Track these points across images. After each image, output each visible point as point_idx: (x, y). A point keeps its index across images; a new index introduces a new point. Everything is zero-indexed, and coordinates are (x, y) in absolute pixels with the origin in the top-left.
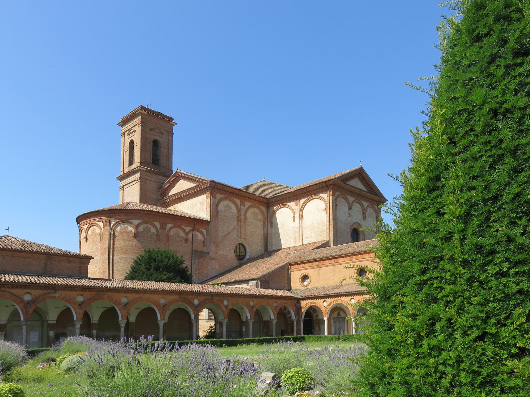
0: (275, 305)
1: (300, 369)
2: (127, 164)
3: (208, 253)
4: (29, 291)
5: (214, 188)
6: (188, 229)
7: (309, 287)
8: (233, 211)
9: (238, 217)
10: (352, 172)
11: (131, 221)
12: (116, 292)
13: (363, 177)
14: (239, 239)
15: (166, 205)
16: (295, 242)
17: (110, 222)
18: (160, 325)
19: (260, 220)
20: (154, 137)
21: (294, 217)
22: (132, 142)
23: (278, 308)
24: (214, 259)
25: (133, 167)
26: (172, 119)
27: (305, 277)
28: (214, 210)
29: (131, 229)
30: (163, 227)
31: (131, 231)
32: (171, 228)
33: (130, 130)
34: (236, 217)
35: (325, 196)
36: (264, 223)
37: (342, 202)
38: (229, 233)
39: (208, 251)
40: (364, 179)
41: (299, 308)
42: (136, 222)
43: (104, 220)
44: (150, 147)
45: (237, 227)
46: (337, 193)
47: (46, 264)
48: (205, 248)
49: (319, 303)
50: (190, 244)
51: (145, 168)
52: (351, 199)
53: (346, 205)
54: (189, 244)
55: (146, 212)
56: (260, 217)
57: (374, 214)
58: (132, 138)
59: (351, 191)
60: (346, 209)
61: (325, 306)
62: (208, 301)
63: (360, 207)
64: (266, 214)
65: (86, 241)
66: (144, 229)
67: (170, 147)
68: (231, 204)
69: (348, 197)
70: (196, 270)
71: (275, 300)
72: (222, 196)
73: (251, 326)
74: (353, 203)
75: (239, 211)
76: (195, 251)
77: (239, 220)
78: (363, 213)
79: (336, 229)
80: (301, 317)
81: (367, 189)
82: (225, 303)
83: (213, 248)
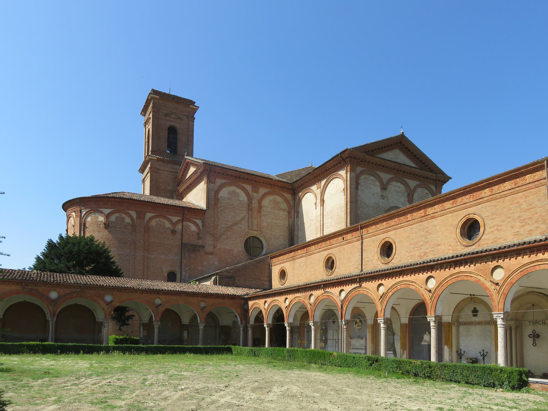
1: (56, 398)
3: (203, 247)
6: (175, 219)
8: (241, 199)
9: (249, 205)
11: (101, 210)
14: (251, 232)
16: (316, 233)
17: (81, 211)
18: (155, 326)
19: (284, 210)
20: (169, 124)
26: (193, 103)
27: (283, 274)
28: (212, 197)
29: (101, 219)
30: (141, 216)
31: (102, 221)
32: (151, 219)
35: (342, 173)
36: (289, 212)
38: (236, 224)
40: (409, 150)
42: (107, 211)
43: (75, 210)
44: (164, 134)
45: (247, 217)
46: (359, 169)
48: (200, 241)
51: (155, 157)
52: (385, 177)
53: (378, 184)
54: (178, 236)
55: (117, 200)
56: (284, 206)
60: (376, 188)
63: (404, 188)
64: (291, 202)
71: (201, 299)
72: (224, 181)
73: (156, 330)
74: (389, 181)
75: (250, 198)
76: (186, 244)
78: (408, 195)
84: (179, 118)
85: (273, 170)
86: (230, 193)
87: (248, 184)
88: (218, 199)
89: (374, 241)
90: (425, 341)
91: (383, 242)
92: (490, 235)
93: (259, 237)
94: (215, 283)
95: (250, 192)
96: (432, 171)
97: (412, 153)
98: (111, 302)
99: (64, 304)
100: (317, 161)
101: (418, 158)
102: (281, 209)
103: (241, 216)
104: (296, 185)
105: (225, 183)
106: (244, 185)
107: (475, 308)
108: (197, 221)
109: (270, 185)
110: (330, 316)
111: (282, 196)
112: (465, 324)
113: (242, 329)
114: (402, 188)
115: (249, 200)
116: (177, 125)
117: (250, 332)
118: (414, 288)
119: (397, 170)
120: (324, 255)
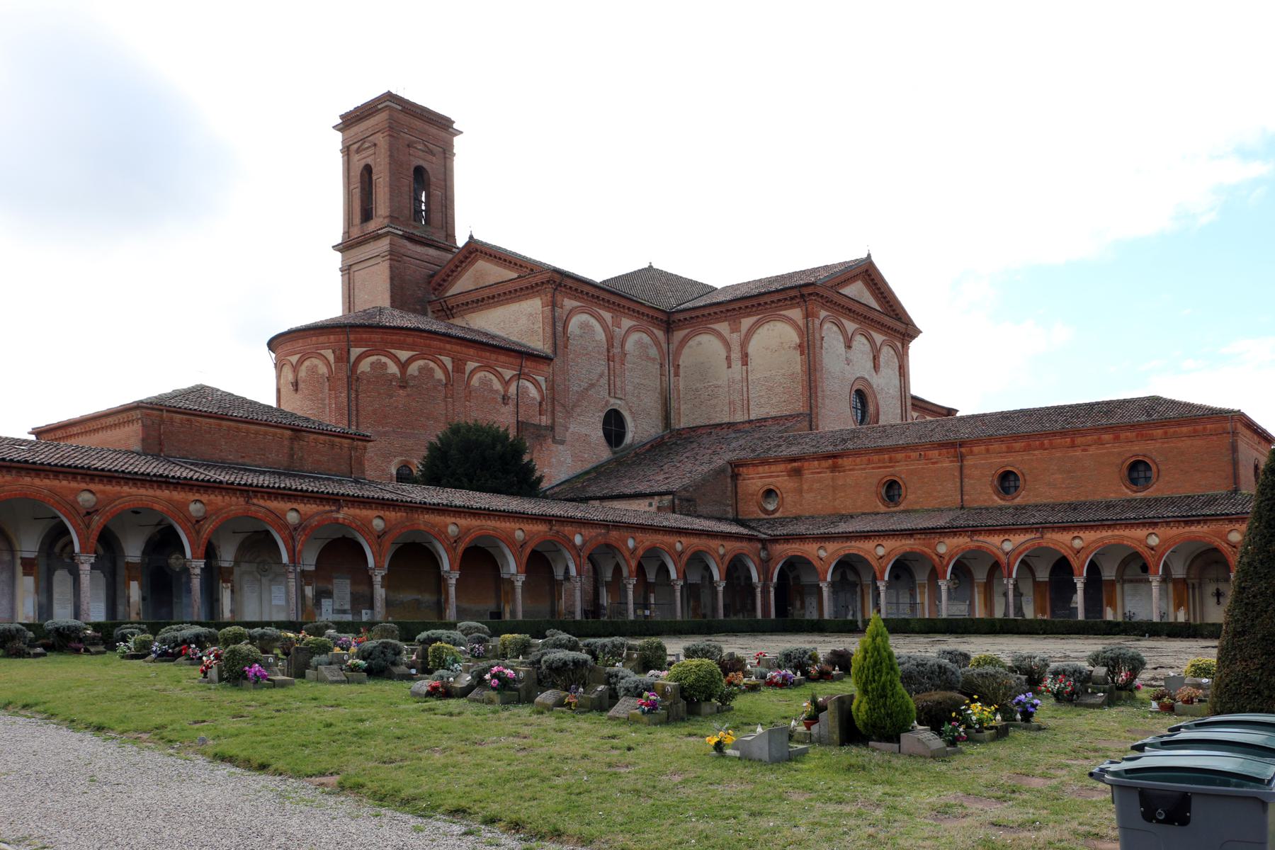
0: (722, 551)
2: (357, 219)
4: (296, 506)
5: (560, 285)
6: (508, 373)
7: (777, 515)
9: (608, 351)
10: (886, 284)
14: (612, 401)
15: (447, 312)
21: (728, 358)
22: (368, 170)
23: (727, 559)
25: (372, 226)
30: (459, 368)
32: (473, 372)
38: (592, 386)
47: (292, 449)
48: (544, 418)
49: (811, 550)
52: (850, 326)
54: (510, 408)
56: (653, 352)
58: (369, 161)
61: (825, 555)
64: (665, 346)
65: (296, 390)
66: (421, 369)
68: (593, 321)
69: (873, 334)
71: (720, 542)
77: (610, 359)
78: (874, 358)
87: (608, 309)
99: (120, 544)
103: (599, 370)
108: (539, 378)
111: (651, 335)
112: (1131, 581)
114: (867, 347)
120: (884, 473)
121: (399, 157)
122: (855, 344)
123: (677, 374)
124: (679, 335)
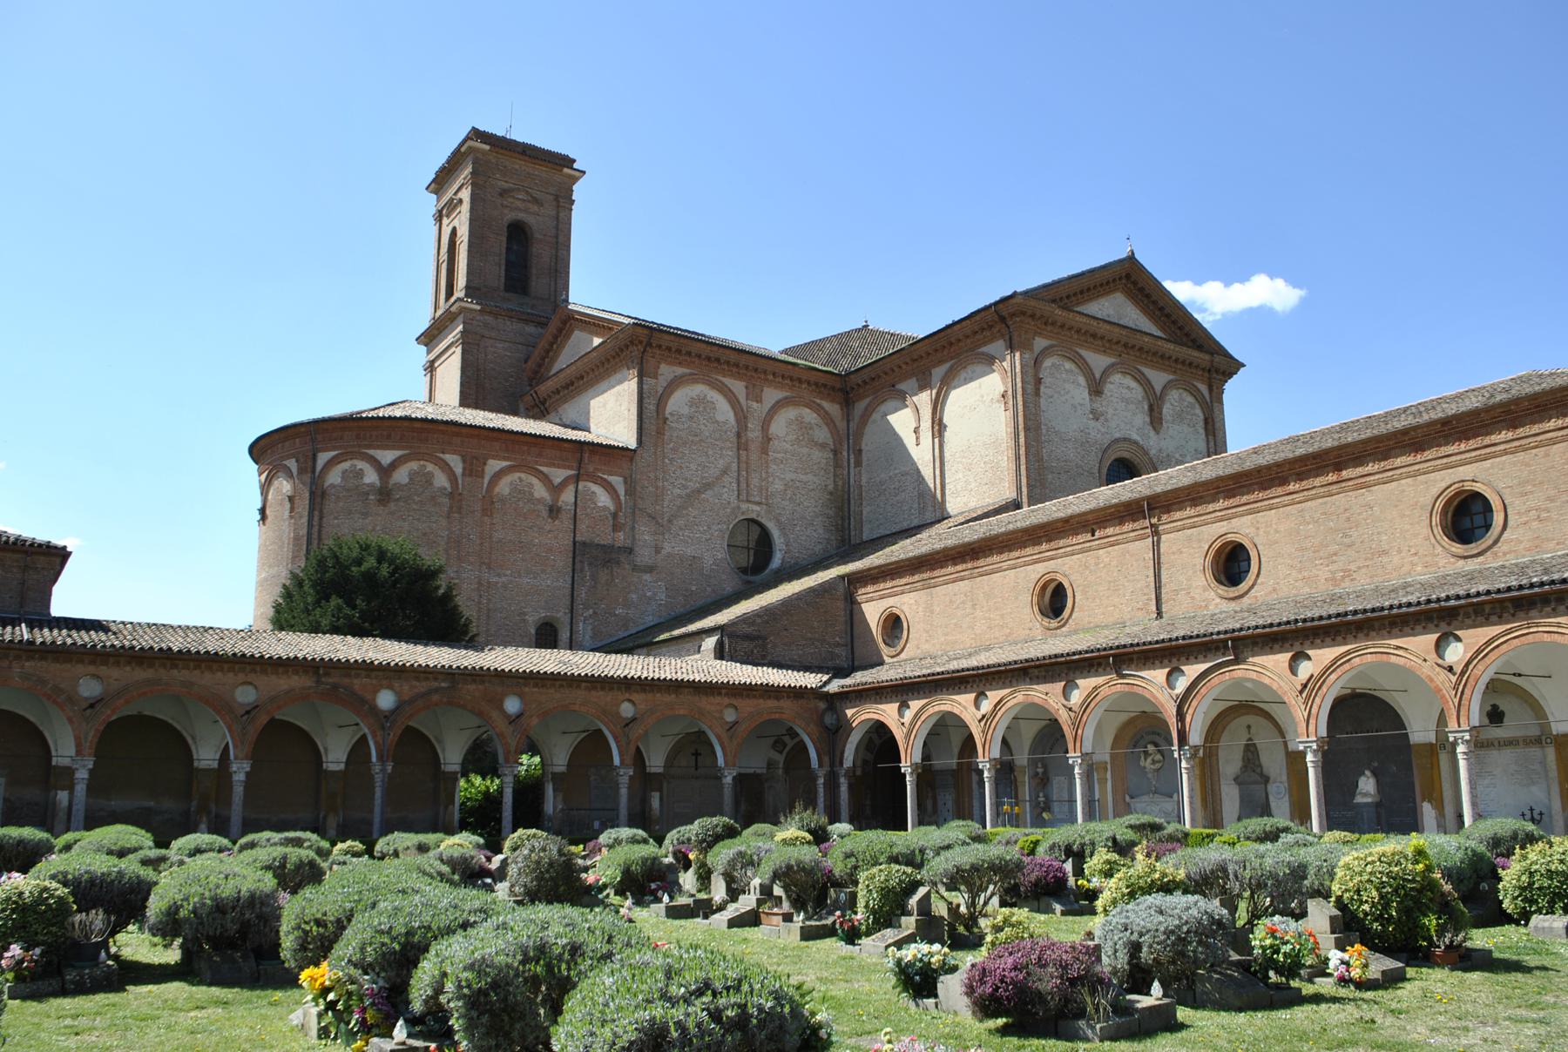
5: (650, 345)
6: (559, 475)
8: (720, 418)
9: (739, 435)
12: (56, 660)
13: (1141, 290)
14: (744, 506)
18: (236, 778)
19: (823, 446)
20: (510, 216)
22: (454, 231)
24: (650, 569)
26: (568, 162)
28: (650, 416)
30: (474, 468)
32: (330, 463)
33: (452, 200)
34: (732, 435)
36: (835, 452)
37: (1067, 388)
38: (708, 486)
39: (628, 543)
41: (840, 729)
44: (499, 243)
45: (734, 466)
48: (621, 535)
49: (887, 713)
50: (568, 524)
52: (1099, 361)
53: (1082, 380)
54: (565, 522)
55: (418, 425)
56: (823, 434)
57: (1198, 411)
59: (1094, 336)
60: (1080, 393)
62: (435, 698)
63: (1140, 389)
64: (841, 425)
66: (412, 475)
67: (561, 239)
69: (1147, 371)
70: (586, 608)
71: (726, 701)
72: (680, 371)
74: (1107, 372)
75: (742, 417)
77: (741, 444)
78: (1151, 408)
79: (1040, 460)
80: (841, 763)
81: (1163, 329)
82: (512, 705)
83: (645, 534)
84: (536, 201)
85: (771, 334)
86: (693, 403)
87: (739, 377)
88: (666, 419)
89: (1189, 539)
90: (1365, 795)
91: (1218, 544)
92: (1521, 531)
93: (763, 521)
94: (720, 653)
95: (742, 397)
96: (1200, 348)
97: (1154, 303)
98: (520, 716)
100: (918, 320)
101: (1168, 316)
102: (816, 444)
103: (721, 463)
104: (854, 379)
105: (682, 376)
106: (728, 381)
107: (1495, 707)
109: (791, 379)
110: (1144, 733)
111: (818, 409)
113: (821, 781)
114: (1137, 391)
115: (738, 421)
116: (530, 220)
117: (844, 789)
118: (1401, 661)
119: (1125, 345)
121: (511, 212)
122: (1109, 389)
123: (858, 464)
124: (860, 406)
